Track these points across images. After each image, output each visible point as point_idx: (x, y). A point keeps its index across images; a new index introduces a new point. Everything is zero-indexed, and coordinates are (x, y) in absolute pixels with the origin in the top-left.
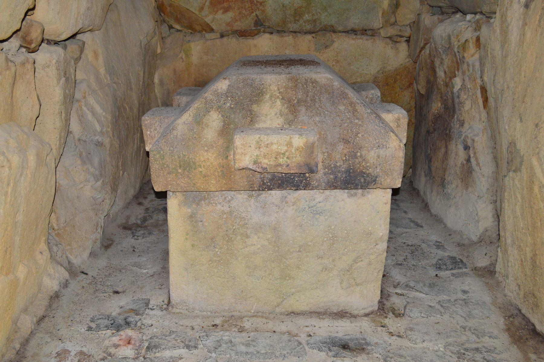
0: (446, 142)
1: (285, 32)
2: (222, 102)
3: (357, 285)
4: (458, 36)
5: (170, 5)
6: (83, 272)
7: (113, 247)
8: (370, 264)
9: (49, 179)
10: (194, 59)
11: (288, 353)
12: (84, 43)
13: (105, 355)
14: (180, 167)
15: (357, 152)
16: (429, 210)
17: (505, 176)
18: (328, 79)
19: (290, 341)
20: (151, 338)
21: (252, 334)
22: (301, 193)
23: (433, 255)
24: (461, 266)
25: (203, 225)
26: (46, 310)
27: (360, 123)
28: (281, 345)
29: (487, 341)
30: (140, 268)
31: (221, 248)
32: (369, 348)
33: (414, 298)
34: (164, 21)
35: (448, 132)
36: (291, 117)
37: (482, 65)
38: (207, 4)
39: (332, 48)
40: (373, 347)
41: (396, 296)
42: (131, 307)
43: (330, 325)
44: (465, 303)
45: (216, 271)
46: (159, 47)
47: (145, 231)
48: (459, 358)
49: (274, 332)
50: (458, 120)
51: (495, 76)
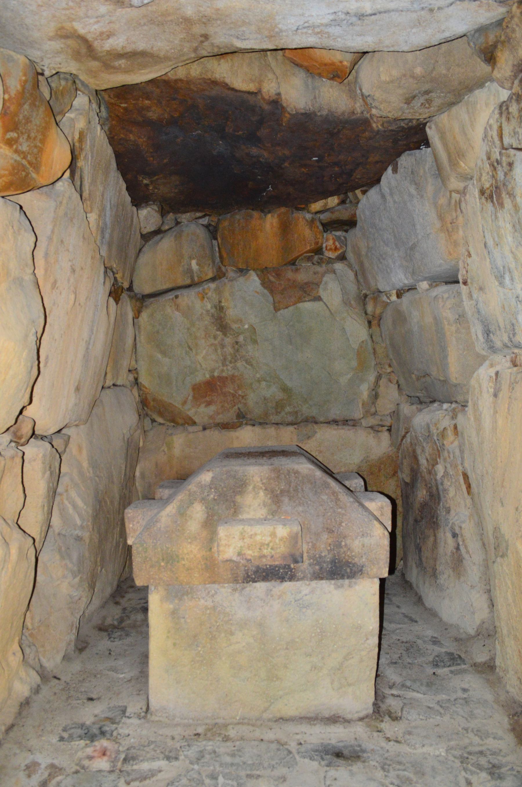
0: (434, 530)
1: (267, 424)
2: (206, 494)
3: (349, 685)
4: (436, 424)
5: (154, 400)
6: (55, 677)
7: (87, 650)
8: (361, 661)
9: (28, 574)
10: (177, 451)
11: (277, 763)
12: (69, 437)
13: (78, 768)
14: (163, 560)
15: (342, 541)
16: (423, 604)
17: (494, 562)
18: (310, 469)
19: (278, 750)
20: (128, 749)
21: (238, 743)
22: (287, 585)
23: (429, 652)
24: (459, 662)
25: (185, 622)
26: (16, 718)
27: (343, 512)
28: (269, 754)
29: (491, 743)
30: (116, 672)
31: (204, 647)
32: (365, 755)
33: (411, 699)
34: (147, 415)
35: (435, 520)
36: (274, 507)
37: (462, 452)
38: (190, 398)
39: (314, 438)
40: (369, 755)
41: (392, 697)
42: (106, 715)
43: (322, 732)
44: (466, 702)
45: (198, 672)
46: (141, 440)
47: (122, 633)
48: (462, 762)
49: (262, 740)
50: (444, 507)
51: (474, 462)
